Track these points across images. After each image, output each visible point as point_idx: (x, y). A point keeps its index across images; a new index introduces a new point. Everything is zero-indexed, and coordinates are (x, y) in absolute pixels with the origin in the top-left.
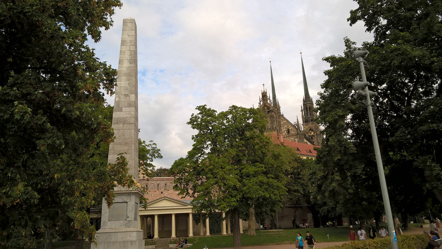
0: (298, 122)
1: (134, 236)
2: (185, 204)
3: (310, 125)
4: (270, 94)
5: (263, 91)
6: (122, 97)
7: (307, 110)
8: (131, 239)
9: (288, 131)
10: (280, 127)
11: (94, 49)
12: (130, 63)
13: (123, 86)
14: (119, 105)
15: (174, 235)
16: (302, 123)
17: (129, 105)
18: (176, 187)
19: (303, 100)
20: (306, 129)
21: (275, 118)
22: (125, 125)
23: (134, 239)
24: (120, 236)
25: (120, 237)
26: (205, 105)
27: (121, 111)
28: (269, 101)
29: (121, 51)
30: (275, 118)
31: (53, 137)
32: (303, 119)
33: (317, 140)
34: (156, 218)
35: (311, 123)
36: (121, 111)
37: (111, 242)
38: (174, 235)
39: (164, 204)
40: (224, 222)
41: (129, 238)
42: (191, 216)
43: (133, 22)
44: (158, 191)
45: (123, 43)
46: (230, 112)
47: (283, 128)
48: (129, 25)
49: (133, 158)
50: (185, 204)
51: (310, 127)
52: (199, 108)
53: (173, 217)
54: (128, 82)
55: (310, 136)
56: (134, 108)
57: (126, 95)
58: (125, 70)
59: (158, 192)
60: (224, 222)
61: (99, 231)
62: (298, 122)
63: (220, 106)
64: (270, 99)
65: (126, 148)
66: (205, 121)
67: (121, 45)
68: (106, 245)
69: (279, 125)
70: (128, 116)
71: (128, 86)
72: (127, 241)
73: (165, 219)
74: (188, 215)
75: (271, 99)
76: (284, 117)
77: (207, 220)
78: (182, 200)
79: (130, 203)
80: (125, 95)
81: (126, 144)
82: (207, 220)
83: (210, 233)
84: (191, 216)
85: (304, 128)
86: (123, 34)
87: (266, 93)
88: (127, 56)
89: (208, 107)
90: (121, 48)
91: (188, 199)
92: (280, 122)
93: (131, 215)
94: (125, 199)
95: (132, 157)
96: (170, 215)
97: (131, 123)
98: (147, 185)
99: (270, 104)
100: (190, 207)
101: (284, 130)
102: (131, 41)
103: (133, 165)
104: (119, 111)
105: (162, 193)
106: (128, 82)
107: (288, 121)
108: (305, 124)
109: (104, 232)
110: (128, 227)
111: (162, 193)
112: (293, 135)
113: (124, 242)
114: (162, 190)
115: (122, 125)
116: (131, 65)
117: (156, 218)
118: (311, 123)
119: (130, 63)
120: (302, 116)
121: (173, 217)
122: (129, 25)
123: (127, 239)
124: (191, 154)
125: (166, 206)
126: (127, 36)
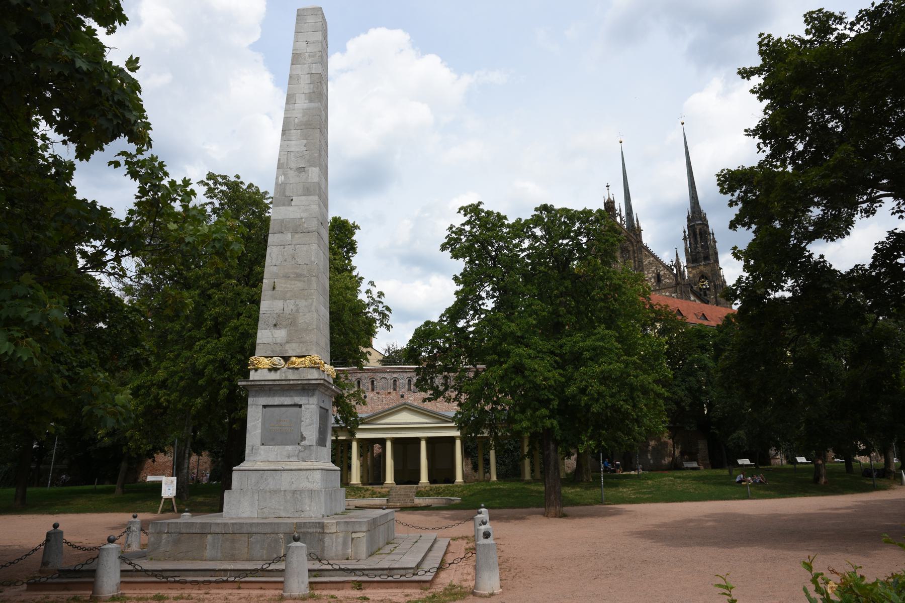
0: (678, 260)
1: (316, 481)
2: (445, 419)
3: (701, 268)
4: (620, 204)
5: (607, 198)
6: (291, 173)
7: (695, 238)
8: (310, 486)
9: (658, 278)
10: (642, 270)
13: (293, 149)
14: (284, 192)
15: (424, 478)
16: (685, 264)
17: (307, 191)
18: (421, 385)
19: (688, 218)
20: (694, 277)
21: (631, 253)
22: (297, 236)
24: (286, 478)
25: (285, 481)
26: (480, 203)
28: (618, 219)
29: (290, 77)
30: (631, 253)
32: (686, 255)
33: (716, 297)
34: (389, 445)
35: (703, 263)
37: (265, 492)
38: (424, 478)
39: (404, 418)
40: (527, 461)
41: (305, 485)
42: (458, 443)
43: (318, 12)
44: (394, 393)
45: (296, 58)
46: (536, 221)
47: (649, 273)
48: (311, 20)
49: (313, 308)
50: (445, 419)
51: (701, 272)
52: (465, 210)
53: (423, 444)
54: (305, 142)
55: (701, 289)
56: (316, 198)
57: (301, 170)
58: (300, 116)
59: (394, 395)
60: (527, 461)
61: (243, 466)
63: (514, 203)
64: (620, 215)
65: (299, 285)
66: (481, 241)
67: (292, 64)
68: (256, 497)
69: (639, 266)
70: (304, 215)
71: (305, 149)
72: (301, 492)
73: (406, 448)
74: (452, 440)
75: (623, 214)
76: (649, 251)
77: (492, 453)
78: (429, 406)
79: (307, 406)
80: (299, 169)
81: (298, 276)
82: (492, 453)
83: (432, 480)
84: (458, 443)
85: (689, 273)
86: (296, 41)
87: (613, 202)
88: (305, 85)
89: (485, 207)
90: (291, 69)
91: (451, 410)
92: (641, 262)
93: (311, 434)
95: (312, 304)
96: (417, 440)
97: (310, 229)
98: (373, 382)
99: (621, 225)
100: (453, 425)
101: (650, 276)
102: (313, 55)
103: (315, 323)
104: (284, 205)
106: (305, 142)
107: (657, 258)
108: (691, 265)
109: (252, 468)
110: (304, 460)
111: (402, 396)
112: (666, 288)
113: (294, 492)
114: (403, 390)
115: (289, 235)
116: (312, 105)
117: (389, 445)
118: (703, 263)
119: (311, 101)
120: (686, 250)
121: (423, 444)
122: (311, 20)
123: (301, 485)
124: (454, 313)
125: (409, 421)
126: (305, 43)
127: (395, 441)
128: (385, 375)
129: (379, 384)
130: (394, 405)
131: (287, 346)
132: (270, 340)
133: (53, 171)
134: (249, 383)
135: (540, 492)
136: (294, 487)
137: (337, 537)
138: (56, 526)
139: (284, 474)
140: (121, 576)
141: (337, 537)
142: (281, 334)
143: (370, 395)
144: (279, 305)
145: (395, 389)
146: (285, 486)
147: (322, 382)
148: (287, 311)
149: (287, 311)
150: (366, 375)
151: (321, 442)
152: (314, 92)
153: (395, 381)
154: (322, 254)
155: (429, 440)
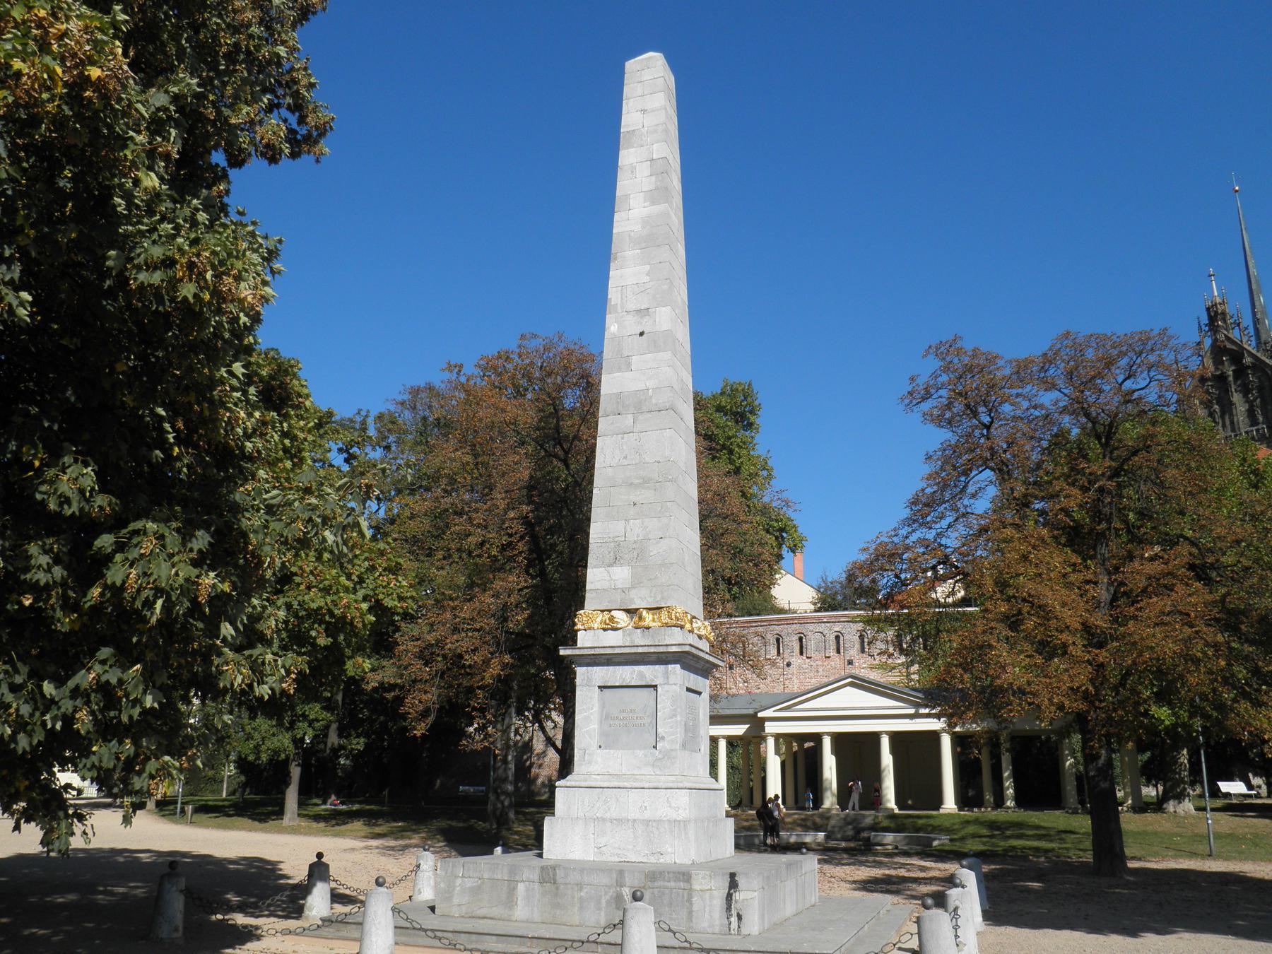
8: (674, 815)
11: (317, 161)
12: (653, 203)
23: (683, 815)
27: (628, 367)
31: (959, 344)
36: (628, 367)
38: (950, 803)
41: (663, 812)
54: (647, 267)
58: (638, 228)
62: (124, 582)
70: (651, 384)
71: (647, 279)
72: (660, 821)
74: (934, 737)
79: (666, 687)
81: (645, 482)
83: (964, 800)
93: (671, 730)
94: (649, 673)
96: (874, 737)
104: (619, 370)
105: (850, 663)
106: (647, 267)
111: (850, 663)
113: (647, 822)
115: (630, 417)
121: (885, 742)
127: (838, 739)
128: (821, 628)
129: (812, 642)
130: (837, 676)
131: (633, 594)
132: (606, 585)
133: (46, 425)
134: (577, 652)
135: (527, 890)
136: (647, 815)
137: (711, 898)
138: (320, 855)
139: (633, 793)
140: (395, 934)
141: (711, 898)
142: (622, 574)
143: (797, 660)
144: (617, 527)
145: (838, 652)
146: (634, 814)
147: (687, 648)
148: (632, 537)
149: (632, 537)
150: (790, 628)
151: (688, 744)
152: (657, 189)
153: (837, 638)
154: (683, 444)
155: (896, 737)
